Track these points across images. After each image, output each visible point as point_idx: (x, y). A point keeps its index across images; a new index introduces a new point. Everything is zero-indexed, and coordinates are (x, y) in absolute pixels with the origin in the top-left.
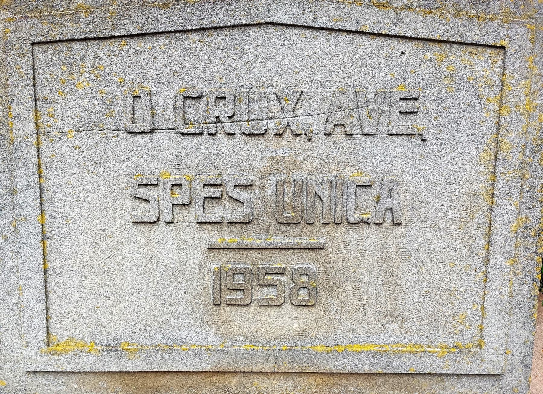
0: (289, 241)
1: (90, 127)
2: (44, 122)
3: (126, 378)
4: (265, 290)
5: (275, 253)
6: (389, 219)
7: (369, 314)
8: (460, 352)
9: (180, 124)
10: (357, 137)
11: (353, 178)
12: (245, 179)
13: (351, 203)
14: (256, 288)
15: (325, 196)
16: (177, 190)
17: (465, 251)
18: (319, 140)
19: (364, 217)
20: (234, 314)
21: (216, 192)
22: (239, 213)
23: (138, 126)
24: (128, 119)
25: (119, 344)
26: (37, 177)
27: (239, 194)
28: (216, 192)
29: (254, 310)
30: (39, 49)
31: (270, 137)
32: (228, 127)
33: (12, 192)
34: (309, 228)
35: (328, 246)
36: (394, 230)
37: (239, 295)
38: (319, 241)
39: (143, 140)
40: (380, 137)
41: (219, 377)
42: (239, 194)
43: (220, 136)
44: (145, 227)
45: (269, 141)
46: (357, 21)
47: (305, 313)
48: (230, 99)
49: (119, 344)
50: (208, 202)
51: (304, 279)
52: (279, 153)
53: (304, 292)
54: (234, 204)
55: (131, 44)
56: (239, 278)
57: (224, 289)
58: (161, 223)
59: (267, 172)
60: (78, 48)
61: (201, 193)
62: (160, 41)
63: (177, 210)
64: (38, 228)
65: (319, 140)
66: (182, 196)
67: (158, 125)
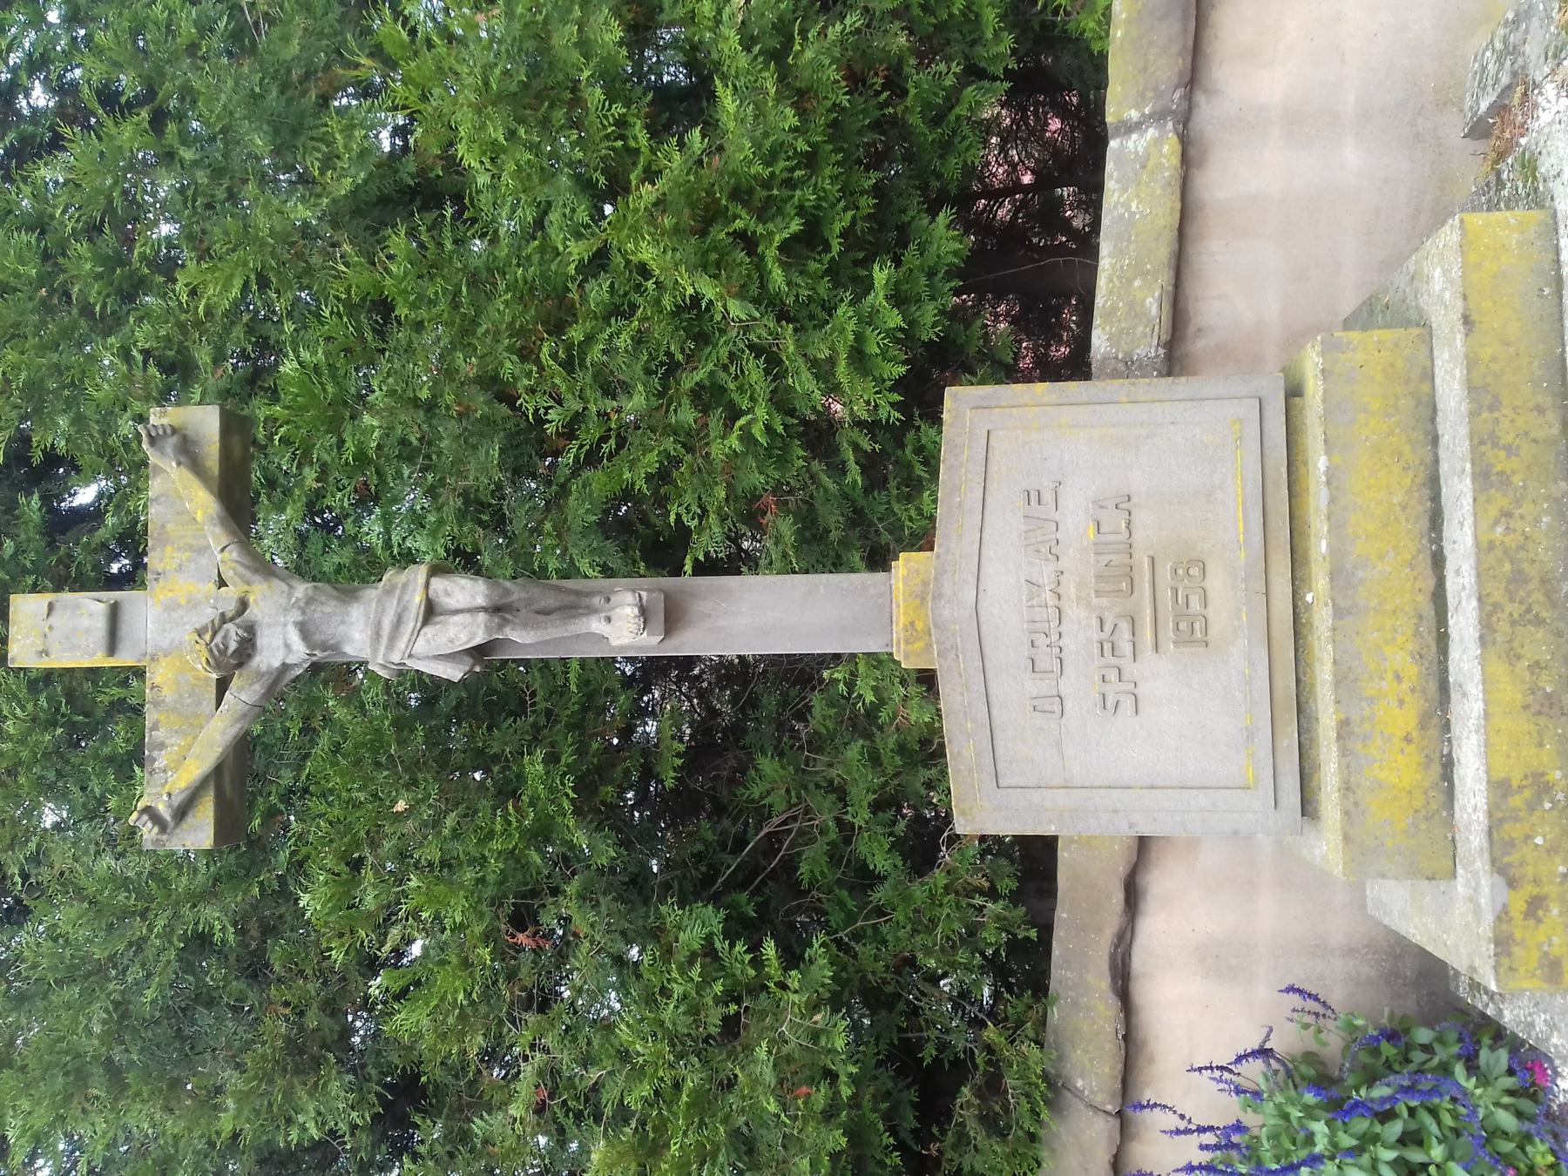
0: (1147, 587)
1: (1059, 745)
2: (1056, 782)
3: (1278, 723)
4: (1192, 604)
5: (1158, 596)
6: (1124, 506)
7: (1209, 515)
8: (1240, 438)
9: (1054, 676)
10: (1059, 535)
11: (1092, 537)
12: (1095, 623)
13: (1112, 538)
14: (1191, 611)
15: (1107, 558)
16: (1107, 679)
17: (1149, 441)
18: (1061, 565)
19: (1123, 525)
20: (1214, 630)
21: (1107, 647)
22: (1125, 627)
23: (1057, 708)
24: (1051, 675)
25: (1247, 728)
26: (1101, 791)
27: (1108, 628)
28: (1107, 647)
29: (1210, 612)
30: (1001, 784)
31: (1061, 604)
32: (1054, 637)
33: (1115, 811)
34: (1135, 569)
35: (1151, 553)
36: (1134, 500)
37: (1197, 626)
38: (1146, 561)
39: (1068, 705)
40: (1057, 516)
41: (1274, 641)
42: (1108, 628)
43: (1061, 643)
44: (1140, 706)
45: (1063, 604)
46: (973, 542)
47: (1210, 568)
48: (1034, 637)
49: (1247, 728)
50: (1116, 653)
51: (1180, 572)
52: (1073, 596)
53: (1191, 572)
54: (1117, 630)
55: (995, 712)
56: (1182, 626)
57: (1192, 639)
58: (1136, 691)
59: (1089, 604)
60: (1000, 752)
61: (1110, 659)
62: (991, 691)
63: (1124, 678)
64: (1145, 791)
65: (1061, 565)
66: (1112, 675)
67: (1055, 693)
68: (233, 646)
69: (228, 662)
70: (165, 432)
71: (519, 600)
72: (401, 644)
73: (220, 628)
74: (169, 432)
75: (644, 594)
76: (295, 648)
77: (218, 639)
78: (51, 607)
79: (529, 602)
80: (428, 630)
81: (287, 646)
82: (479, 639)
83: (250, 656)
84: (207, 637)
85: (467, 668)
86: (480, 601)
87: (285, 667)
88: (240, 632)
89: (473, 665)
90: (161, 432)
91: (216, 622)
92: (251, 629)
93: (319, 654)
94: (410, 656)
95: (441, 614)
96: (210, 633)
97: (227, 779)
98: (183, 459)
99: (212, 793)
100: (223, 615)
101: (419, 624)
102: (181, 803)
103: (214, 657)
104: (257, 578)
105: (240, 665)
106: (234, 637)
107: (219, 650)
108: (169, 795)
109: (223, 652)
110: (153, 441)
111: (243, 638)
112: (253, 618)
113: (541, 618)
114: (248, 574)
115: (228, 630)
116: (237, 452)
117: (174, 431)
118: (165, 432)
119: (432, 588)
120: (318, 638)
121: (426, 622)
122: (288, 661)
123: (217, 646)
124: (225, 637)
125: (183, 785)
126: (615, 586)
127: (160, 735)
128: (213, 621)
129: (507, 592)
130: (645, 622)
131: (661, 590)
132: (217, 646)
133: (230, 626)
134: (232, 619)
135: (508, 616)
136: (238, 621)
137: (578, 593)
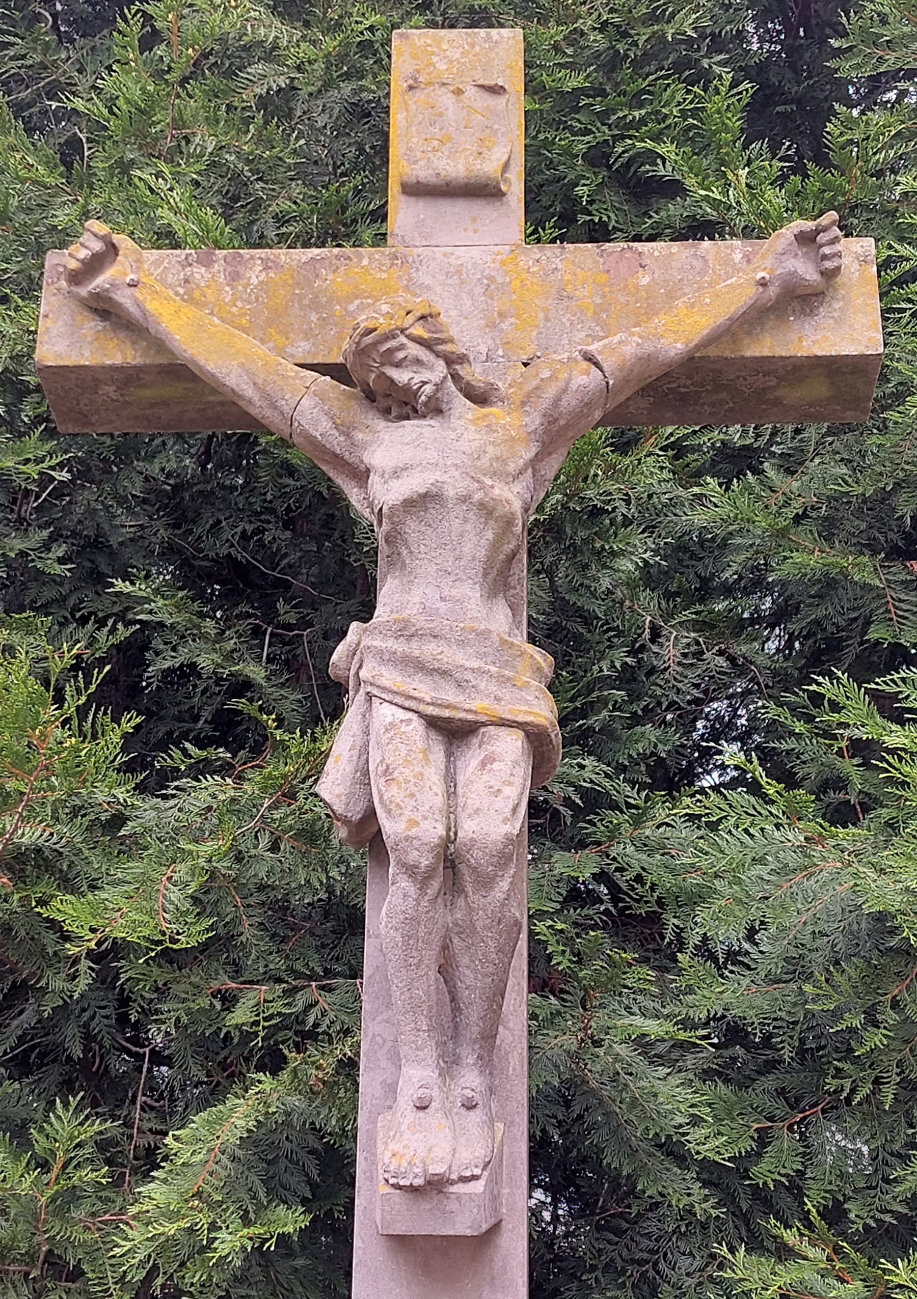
68: (401, 376)
69: (370, 369)
70: (825, 257)
71: (470, 910)
72: (390, 677)
73: (438, 355)
74: (828, 264)
75: (478, 1187)
76: (395, 484)
77: (415, 350)
78: (496, 90)
79: (467, 930)
80: (417, 726)
81: (396, 474)
82: (390, 827)
83: (386, 412)
84: (418, 330)
85: (339, 808)
86: (468, 829)
87: (362, 475)
88: (428, 389)
89: (346, 822)
90: (827, 250)
91: (448, 348)
92: (435, 409)
93: (381, 532)
94: (369, 696)
95: (449, 754)
96: (426, 335)
97: (169, 390)
98: (773, 291)
99: (139, 361)
100: (463, 359)
101: (431, 710)
102: (119, 306)
103: (375, 344)
104: (534, 420)
105: (370, 396)
106: (417, 379)
107: (390, 351)
108: (133, 285)
109: (388, 358)
110: (806, 239)
111: (416, 394)
112: (455, 412)
113: (431, 957)
114: (545, 403)
115: (431, 368)
116: (793, 395)
117: (830, 275)
118: (825, 257)
119: (503, 732)
120: (412, 527)
121: (433, 723)
122: (374, 478)
123: (402, 347)
124: (418, 362)
125: (152, 306)
126: (508, 1125)
127: (255, 275)
128: (452, 341)
129: (486, 883)
130: (413, 1189)
131: (495, 1229)
132: (402, 347)
133: (441, 368)
134: (456, 378)
135: (436, 884)
136: (450, 383)
137: (489, 1037)
